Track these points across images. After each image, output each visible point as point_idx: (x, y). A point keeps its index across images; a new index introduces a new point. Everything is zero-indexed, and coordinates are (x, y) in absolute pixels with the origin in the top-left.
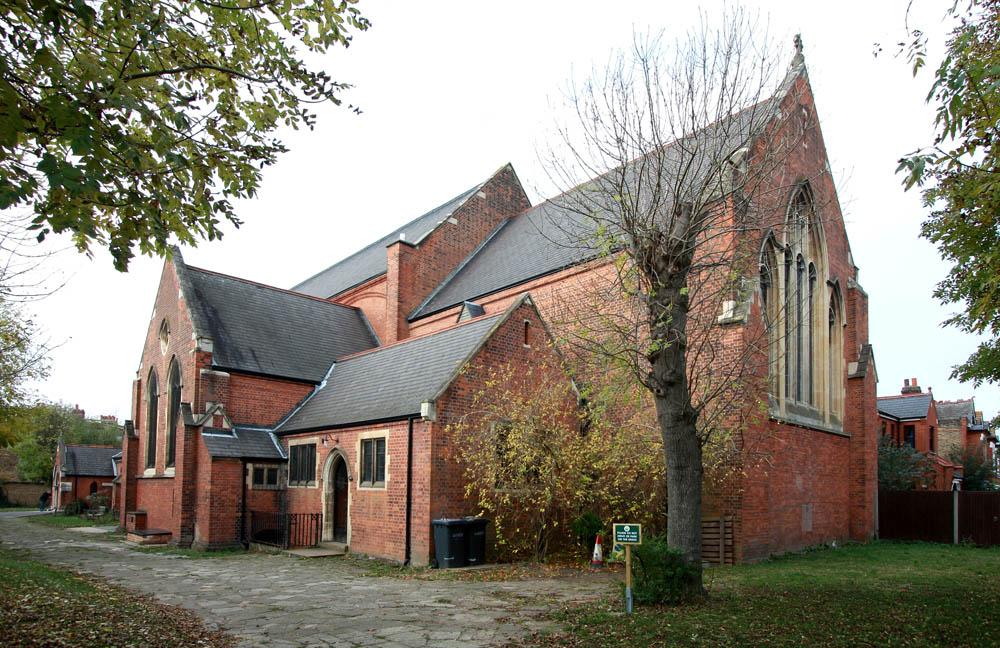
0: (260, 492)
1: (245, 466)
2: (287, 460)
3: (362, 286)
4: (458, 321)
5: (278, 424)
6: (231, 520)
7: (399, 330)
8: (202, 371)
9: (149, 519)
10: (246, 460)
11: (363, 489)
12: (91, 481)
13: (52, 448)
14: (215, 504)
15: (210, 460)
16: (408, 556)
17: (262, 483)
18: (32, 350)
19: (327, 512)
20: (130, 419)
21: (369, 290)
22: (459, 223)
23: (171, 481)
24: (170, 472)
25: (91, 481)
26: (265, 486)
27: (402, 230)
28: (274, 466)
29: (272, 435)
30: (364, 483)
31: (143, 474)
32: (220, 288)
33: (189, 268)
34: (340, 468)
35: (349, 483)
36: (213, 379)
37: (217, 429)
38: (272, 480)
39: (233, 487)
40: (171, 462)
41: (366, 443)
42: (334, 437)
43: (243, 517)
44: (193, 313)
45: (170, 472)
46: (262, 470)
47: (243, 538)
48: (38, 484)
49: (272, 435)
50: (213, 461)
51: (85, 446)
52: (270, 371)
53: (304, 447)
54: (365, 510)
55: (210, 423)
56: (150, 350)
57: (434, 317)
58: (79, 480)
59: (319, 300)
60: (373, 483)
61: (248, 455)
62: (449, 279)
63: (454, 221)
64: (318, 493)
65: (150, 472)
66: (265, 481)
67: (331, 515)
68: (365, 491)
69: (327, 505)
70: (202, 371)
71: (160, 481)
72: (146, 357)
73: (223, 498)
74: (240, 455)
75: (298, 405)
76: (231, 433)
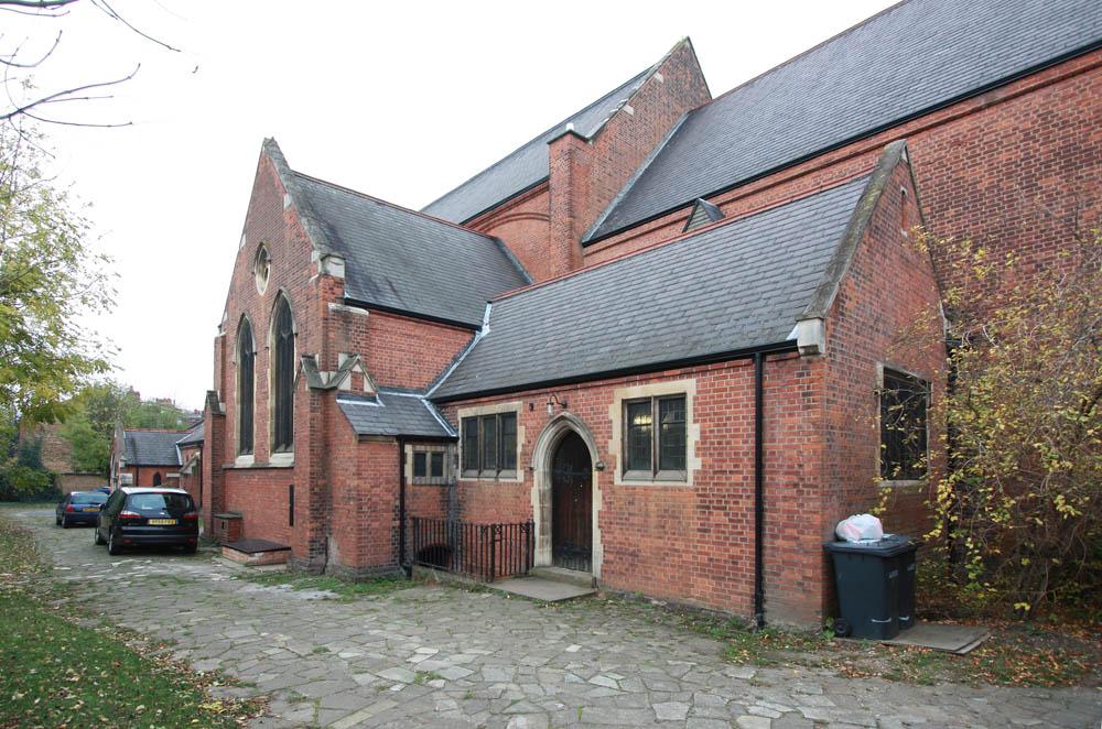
0: (423, 489)
1: (402, 448)
2: (457, 438)
3: (503, 206)
4: (685, 230)
5: (430, 388)
6: (386, 532)
7: (571, 255)
8: (332, 306)
9: (247, 526)
10: (403, 439)
11: (625, 483)
12: (153, 472)
13: (108, 434)
14: (365, 509)
15: (354, 441)
16: (759, 601)
17: (424, 475)
18: (87, 264)
19: (543, 520)
20: (212, 389)
21: (512, 212)
22: (636, 112)
23: (288, 473)
24: (281, 459)
25: (153, 472)
26: (428, 478)
27: (569, 120)
28: (440, 449)
29: (426, 403)
30: (630, 473)
31: (233, 463)
32: (331, 201)
33: (297, 175)
34: (571, 456)
35: (595, 474)
36: (347, 318)
37: (356, 394)
38: (437, 471)
39: (388, 482)
40: (284, 438)
41: (633, 407)
42: (561, 397)
43: (402, 527)
44: (310, 225)
45: (281, 459)
46: (424, 455)
47: (402, 560)
48: (94, 475)
49: (424, 401)
50: (360, 441)
51: (145, 430)
52: (418, 310)
53: (489, 418)
54: (635, 520)
55: (346, 385)
56: (239, 291)
57: (628, 234)
58: (140, 470)
59: (450, 225)
60: (655, 473)
61: (406, 432)
62: (626, 188)
63: (629, 110)
64: (523, 490)
65: (246, 461)
66: (429, 471)
67: (548, 524)
68: (634, 488)
69: (542, 508)
70: (332, 306)
71: (263, 472)
72: (232, 304)
73: (374, 499)
74: (396, 432)
75: (455, 359)
76: (374, 400)
